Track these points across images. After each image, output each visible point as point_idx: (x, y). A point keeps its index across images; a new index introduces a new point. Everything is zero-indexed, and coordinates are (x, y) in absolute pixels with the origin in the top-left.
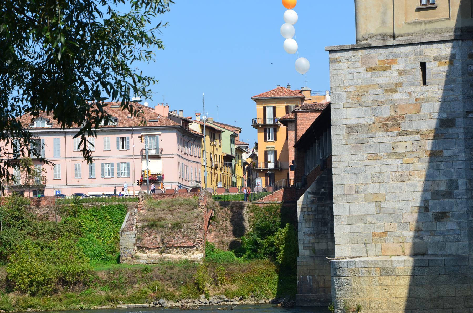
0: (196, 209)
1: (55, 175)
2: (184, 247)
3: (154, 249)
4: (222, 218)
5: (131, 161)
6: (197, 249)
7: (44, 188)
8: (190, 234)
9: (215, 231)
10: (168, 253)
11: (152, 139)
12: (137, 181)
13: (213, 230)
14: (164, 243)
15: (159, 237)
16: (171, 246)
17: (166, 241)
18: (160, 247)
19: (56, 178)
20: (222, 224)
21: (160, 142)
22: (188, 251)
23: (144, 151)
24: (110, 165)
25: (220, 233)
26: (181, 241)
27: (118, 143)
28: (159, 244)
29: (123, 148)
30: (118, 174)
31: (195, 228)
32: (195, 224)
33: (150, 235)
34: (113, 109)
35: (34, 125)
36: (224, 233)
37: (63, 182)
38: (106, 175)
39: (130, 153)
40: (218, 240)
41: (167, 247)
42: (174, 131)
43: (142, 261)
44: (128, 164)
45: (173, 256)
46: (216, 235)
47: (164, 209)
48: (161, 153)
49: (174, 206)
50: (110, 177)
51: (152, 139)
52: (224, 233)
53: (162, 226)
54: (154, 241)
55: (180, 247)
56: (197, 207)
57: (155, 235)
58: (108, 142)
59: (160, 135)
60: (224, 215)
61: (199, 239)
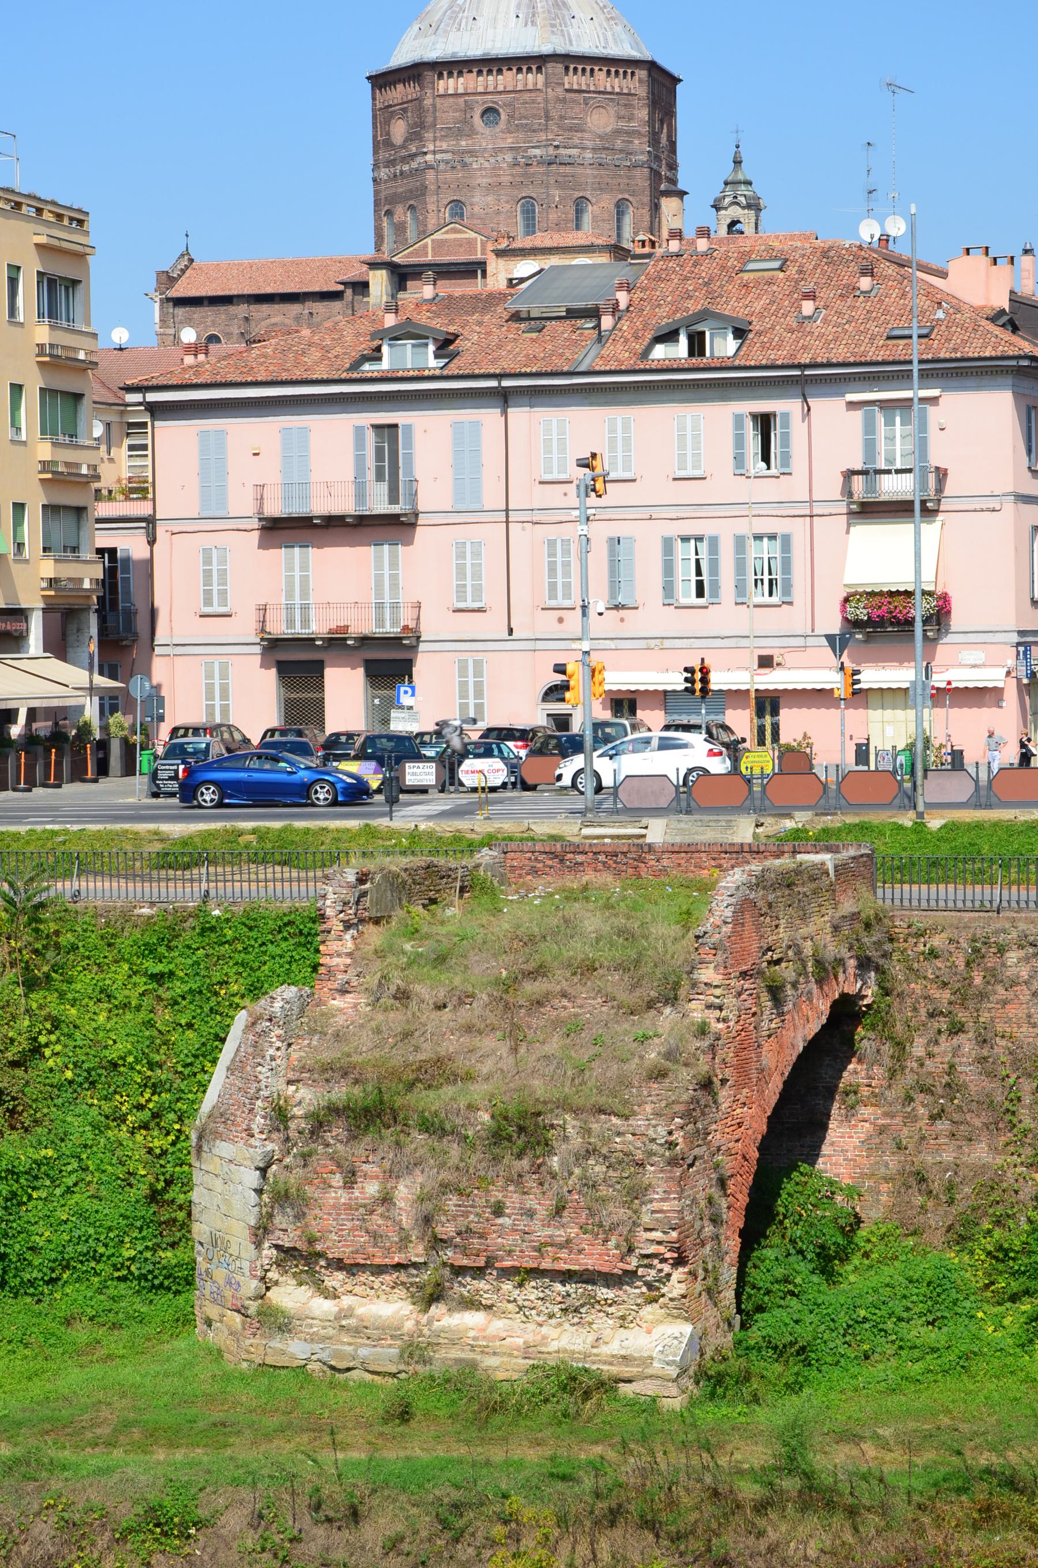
0: (668, 1010)
1: (461, 590)
2: (567, 1276)
3: (379, 1270)
4: (931, 1015)
5: (798, 530)
6: (653, 1293)
7: (414, 648)
8: (604, 1191)
9: (876, 1099)
10: (471, 1304)
11: (898, 419)
12: (686, 670)
13: (865, 1092)
14: (437, 1243)
15: (404, 1192)
16: (481, 1262)
17: (446, 1229)
18: (415, 1265)
19: (462, 605)
20: (931, 1055)
21: (933, 435)
22: (592, 1302)
23: (858, 482)
24: (703, 547)
25: (911, 1118)
26: (543, 1233)
27: (739, 441)
28: (404, 1241)
29: (766, 458)
30: (740, 588)
31: (639, 1155)
32: (638, 1123)
33: (351, 1178)
34: (752, 275)
35: (380, 359)
36: (933, 1118)
37: (493, 625)
38: (687, 595)
39: (795, 487)
40: (893, 1162)
41: (459, 1271)
42: (1000, 380)
43: (296, 1349)
44: (786, 541)
45: (498, 1326)
46: (882, 1130)
47: (472, 996)
48: (940, 490)
49: (539, 972)
50: (701, 601)
51: (898, 419)
52: (933, 1118)
53: (427, 1127)
54: (376, 1221)
55: (536, 1273)
56: (682, 993)
57: (386, 1180)
58: (696, 438)
59: (934, 400)
60: (946, 995)
61: (657, 1235)
